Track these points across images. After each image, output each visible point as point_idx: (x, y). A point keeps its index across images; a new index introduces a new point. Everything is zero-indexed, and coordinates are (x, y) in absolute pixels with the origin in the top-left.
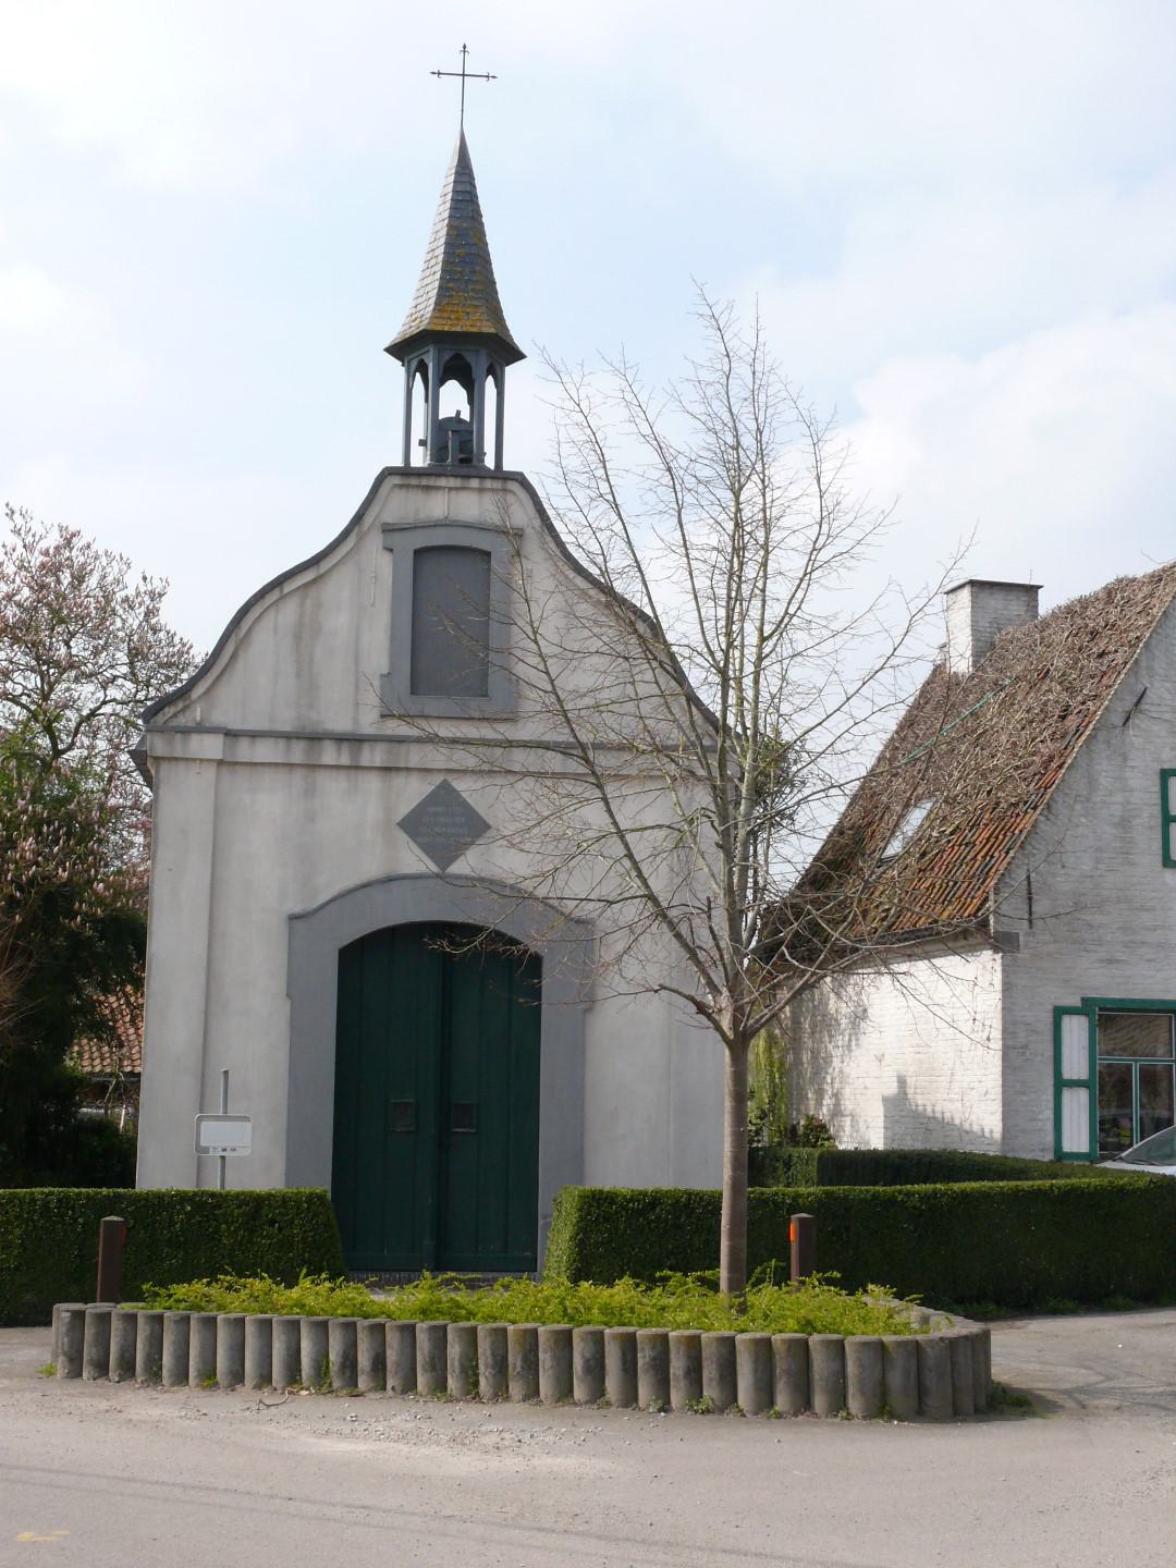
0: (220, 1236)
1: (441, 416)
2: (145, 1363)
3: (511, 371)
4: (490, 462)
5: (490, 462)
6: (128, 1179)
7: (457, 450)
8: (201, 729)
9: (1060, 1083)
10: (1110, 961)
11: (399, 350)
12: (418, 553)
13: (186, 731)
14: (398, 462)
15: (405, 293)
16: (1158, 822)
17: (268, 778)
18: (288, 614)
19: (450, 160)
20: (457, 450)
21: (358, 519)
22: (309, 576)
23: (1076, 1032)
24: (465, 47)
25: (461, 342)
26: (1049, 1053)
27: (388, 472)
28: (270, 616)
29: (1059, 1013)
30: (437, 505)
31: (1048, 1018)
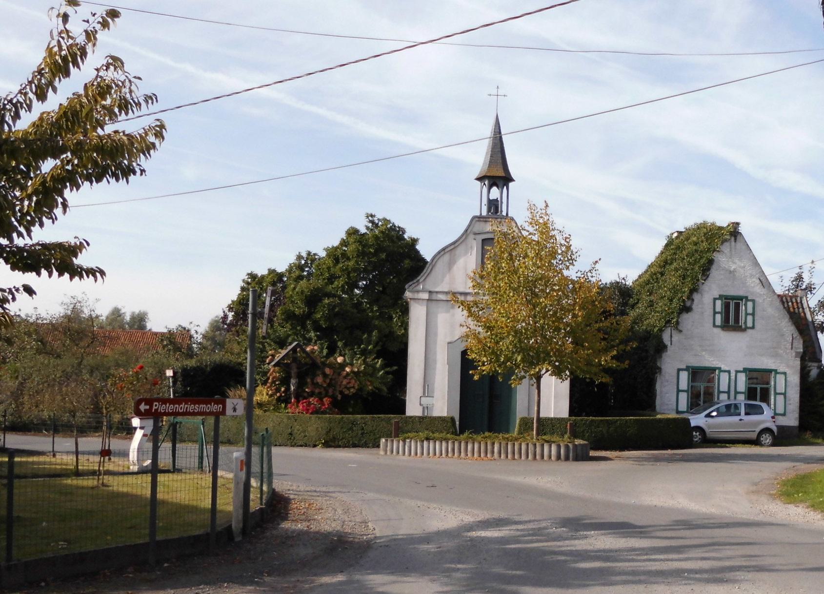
0: (429, 427)
1: (541, 415)
2: (392, 573)
3: (511, 184)
4: (504, 214)
5: (504, 214)
6: (403, 411)
7: (494, 206)
8: (423, 291)
9: (678, 391)
10: (696, 355)
11: (480, 179)
12: (483, 240)
13: (418, 292)
14: (478, 214)
15: (478, 158)
16: (712, 313)
17: (441, 304)
18: (446, 257)
19: (492, 122)
20: (494, 206)
21: (466, 231)
22: (452, 247)
23: (684, 376)
24: (114, 14)
25: (498, 175)
26: (676, 382)
27: (474, 217)
28: (441, 259)
29: (679, 370)
30: (488, 227)
31: (675, 373)
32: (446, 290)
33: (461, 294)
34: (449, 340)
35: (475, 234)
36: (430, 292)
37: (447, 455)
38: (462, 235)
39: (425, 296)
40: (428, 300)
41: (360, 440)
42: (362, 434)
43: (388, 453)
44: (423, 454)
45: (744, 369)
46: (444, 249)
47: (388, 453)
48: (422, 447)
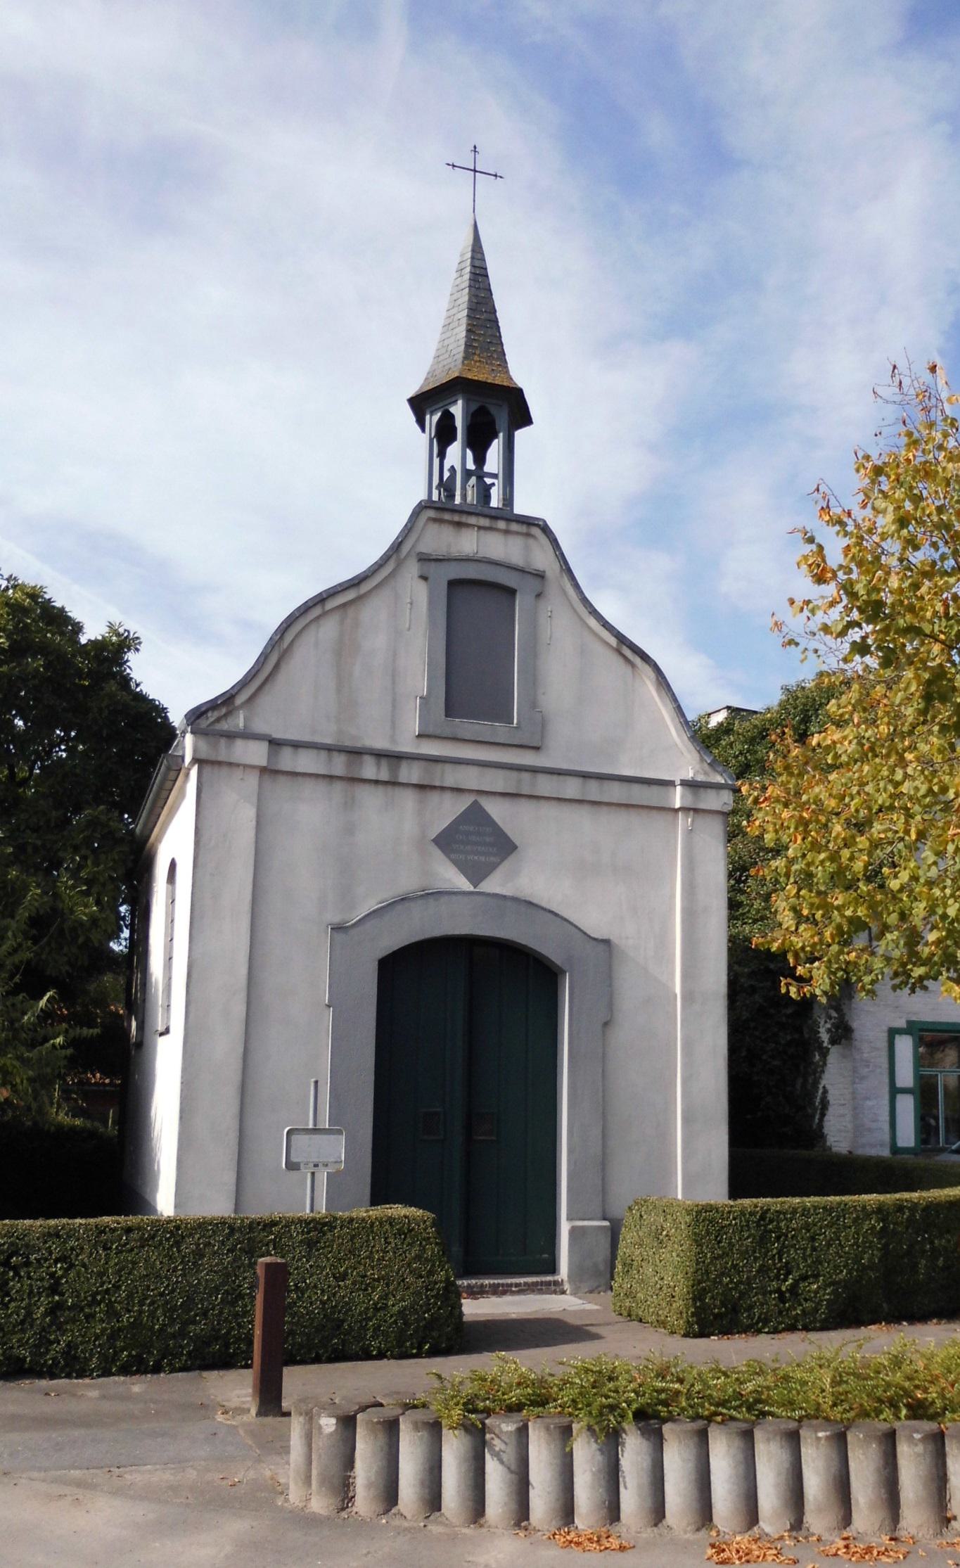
3: (521, 435)
8: (248, 735)
9: (894, 1091)
12: (453, 584)
13: (231, 736)
15: (424, 345)
18: (328, 630)
21: (397, 547)
22: (351, 595)
23: (905, 1046)
26: (886, 1065)
32: (328, 741)
33: (379, 755)
34: (337, 919)
35: (424, 559)
36: (275, 744)
37: (797, 1524)
38: (385, 559)
39: (256, 753)
40: (264, 770)
41: (44, 1342)
42: (54, 1310)
43: (364, 1501)
44: (613, 1511)
45: (910, 1023)
46: (320, 599)
47: (364, 1501)
48: (612, 1476)
